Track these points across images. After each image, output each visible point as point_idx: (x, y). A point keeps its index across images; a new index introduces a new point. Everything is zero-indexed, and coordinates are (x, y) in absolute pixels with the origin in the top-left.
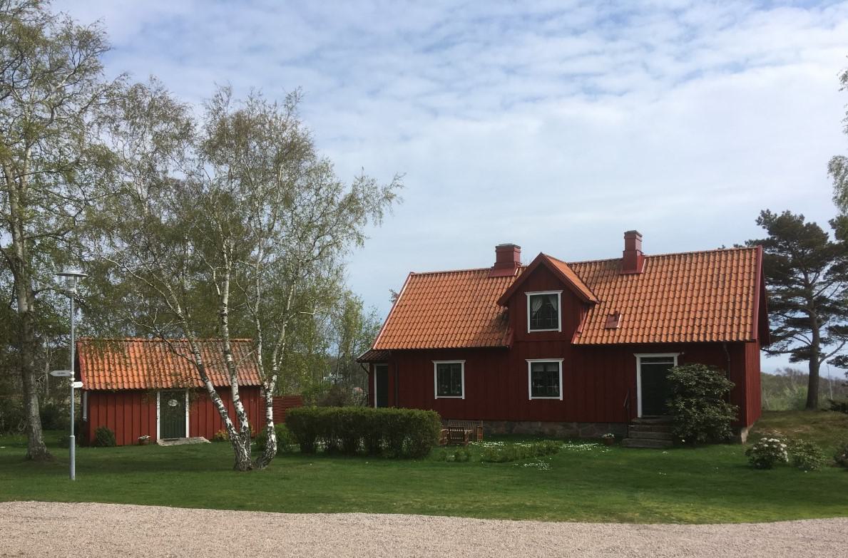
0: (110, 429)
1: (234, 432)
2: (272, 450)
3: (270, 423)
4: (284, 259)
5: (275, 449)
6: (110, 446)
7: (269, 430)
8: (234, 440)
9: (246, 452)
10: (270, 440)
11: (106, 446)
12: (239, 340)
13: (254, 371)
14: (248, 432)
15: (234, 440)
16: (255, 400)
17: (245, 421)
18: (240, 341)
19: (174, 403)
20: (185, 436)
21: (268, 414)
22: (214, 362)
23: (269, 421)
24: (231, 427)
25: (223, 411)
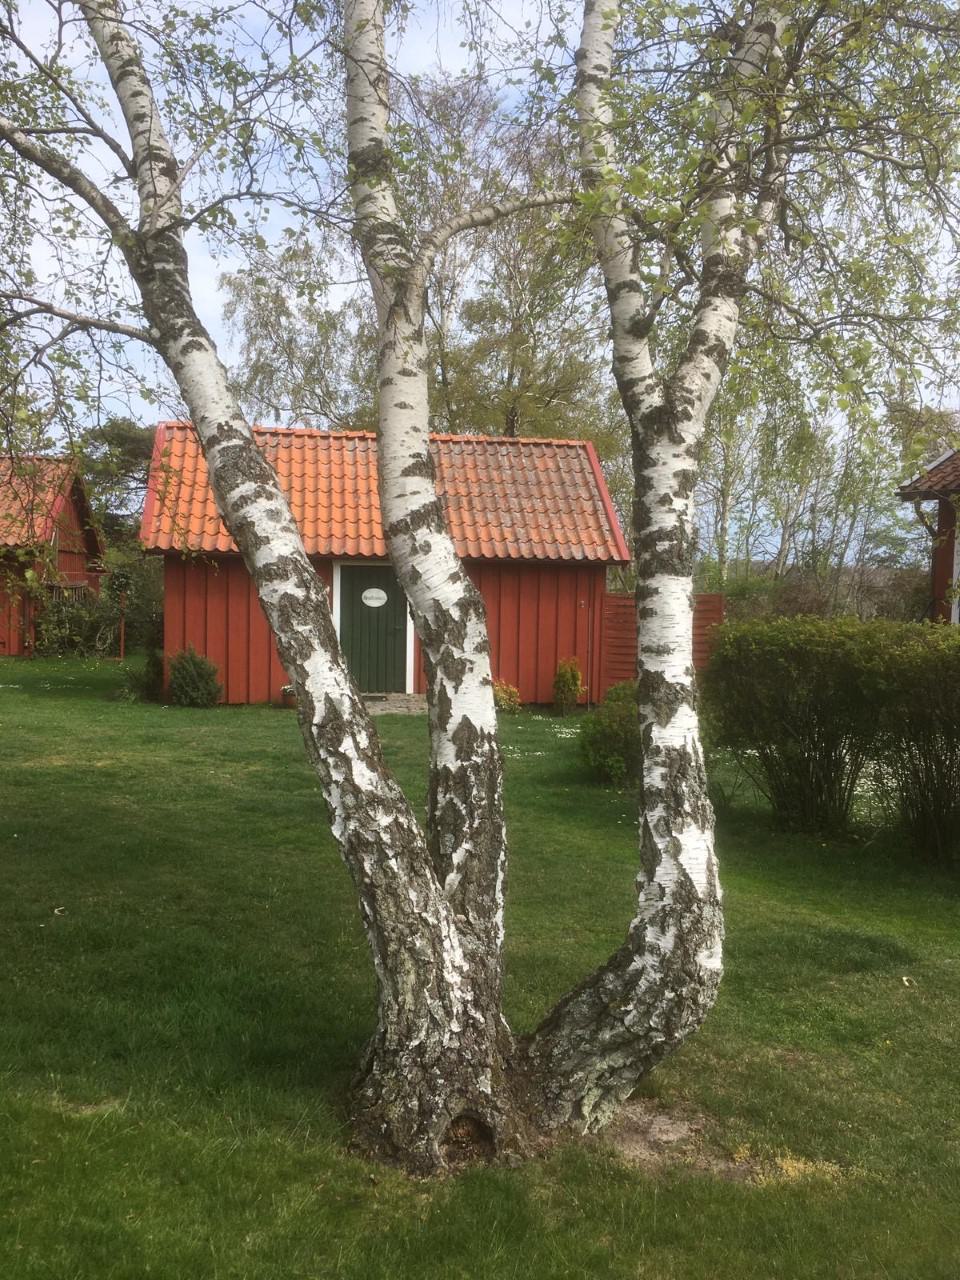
0: (212, 662)
1: (364, 777)
2: (680, 970)
3: (666, 716)
4: (522, 1261)
5: (711, 960)
6: (205, 706)
7: (655, 778)
8: (357, 844)
9: (454, 954)
10: (665, 874)
11: (193, 704)
12: (555, 442)
13: (591, 522)
14: (491, 767)
15: (357, 844)
16: (591, 604)
17: (470, 681)
18: (559, 446)
19: (375, 598)
20: (403, 690)
21: (653, 632)
22: (475, 490)
23: (654, 694)
24: (335, 725)
25: (289, 587)
